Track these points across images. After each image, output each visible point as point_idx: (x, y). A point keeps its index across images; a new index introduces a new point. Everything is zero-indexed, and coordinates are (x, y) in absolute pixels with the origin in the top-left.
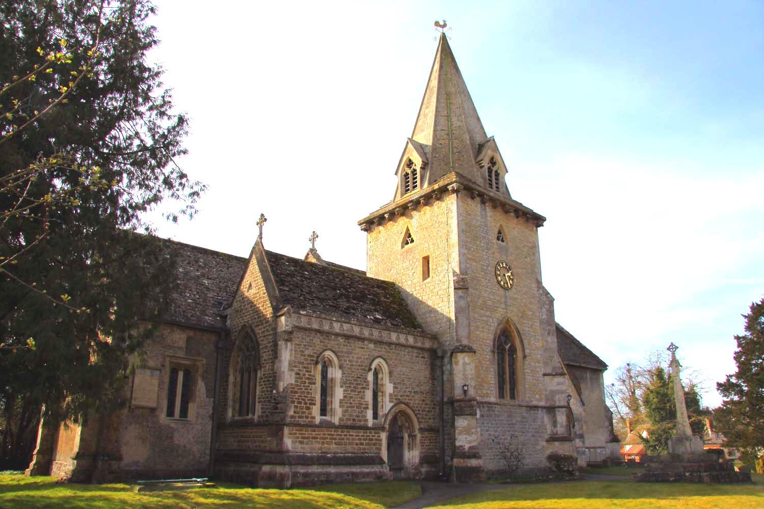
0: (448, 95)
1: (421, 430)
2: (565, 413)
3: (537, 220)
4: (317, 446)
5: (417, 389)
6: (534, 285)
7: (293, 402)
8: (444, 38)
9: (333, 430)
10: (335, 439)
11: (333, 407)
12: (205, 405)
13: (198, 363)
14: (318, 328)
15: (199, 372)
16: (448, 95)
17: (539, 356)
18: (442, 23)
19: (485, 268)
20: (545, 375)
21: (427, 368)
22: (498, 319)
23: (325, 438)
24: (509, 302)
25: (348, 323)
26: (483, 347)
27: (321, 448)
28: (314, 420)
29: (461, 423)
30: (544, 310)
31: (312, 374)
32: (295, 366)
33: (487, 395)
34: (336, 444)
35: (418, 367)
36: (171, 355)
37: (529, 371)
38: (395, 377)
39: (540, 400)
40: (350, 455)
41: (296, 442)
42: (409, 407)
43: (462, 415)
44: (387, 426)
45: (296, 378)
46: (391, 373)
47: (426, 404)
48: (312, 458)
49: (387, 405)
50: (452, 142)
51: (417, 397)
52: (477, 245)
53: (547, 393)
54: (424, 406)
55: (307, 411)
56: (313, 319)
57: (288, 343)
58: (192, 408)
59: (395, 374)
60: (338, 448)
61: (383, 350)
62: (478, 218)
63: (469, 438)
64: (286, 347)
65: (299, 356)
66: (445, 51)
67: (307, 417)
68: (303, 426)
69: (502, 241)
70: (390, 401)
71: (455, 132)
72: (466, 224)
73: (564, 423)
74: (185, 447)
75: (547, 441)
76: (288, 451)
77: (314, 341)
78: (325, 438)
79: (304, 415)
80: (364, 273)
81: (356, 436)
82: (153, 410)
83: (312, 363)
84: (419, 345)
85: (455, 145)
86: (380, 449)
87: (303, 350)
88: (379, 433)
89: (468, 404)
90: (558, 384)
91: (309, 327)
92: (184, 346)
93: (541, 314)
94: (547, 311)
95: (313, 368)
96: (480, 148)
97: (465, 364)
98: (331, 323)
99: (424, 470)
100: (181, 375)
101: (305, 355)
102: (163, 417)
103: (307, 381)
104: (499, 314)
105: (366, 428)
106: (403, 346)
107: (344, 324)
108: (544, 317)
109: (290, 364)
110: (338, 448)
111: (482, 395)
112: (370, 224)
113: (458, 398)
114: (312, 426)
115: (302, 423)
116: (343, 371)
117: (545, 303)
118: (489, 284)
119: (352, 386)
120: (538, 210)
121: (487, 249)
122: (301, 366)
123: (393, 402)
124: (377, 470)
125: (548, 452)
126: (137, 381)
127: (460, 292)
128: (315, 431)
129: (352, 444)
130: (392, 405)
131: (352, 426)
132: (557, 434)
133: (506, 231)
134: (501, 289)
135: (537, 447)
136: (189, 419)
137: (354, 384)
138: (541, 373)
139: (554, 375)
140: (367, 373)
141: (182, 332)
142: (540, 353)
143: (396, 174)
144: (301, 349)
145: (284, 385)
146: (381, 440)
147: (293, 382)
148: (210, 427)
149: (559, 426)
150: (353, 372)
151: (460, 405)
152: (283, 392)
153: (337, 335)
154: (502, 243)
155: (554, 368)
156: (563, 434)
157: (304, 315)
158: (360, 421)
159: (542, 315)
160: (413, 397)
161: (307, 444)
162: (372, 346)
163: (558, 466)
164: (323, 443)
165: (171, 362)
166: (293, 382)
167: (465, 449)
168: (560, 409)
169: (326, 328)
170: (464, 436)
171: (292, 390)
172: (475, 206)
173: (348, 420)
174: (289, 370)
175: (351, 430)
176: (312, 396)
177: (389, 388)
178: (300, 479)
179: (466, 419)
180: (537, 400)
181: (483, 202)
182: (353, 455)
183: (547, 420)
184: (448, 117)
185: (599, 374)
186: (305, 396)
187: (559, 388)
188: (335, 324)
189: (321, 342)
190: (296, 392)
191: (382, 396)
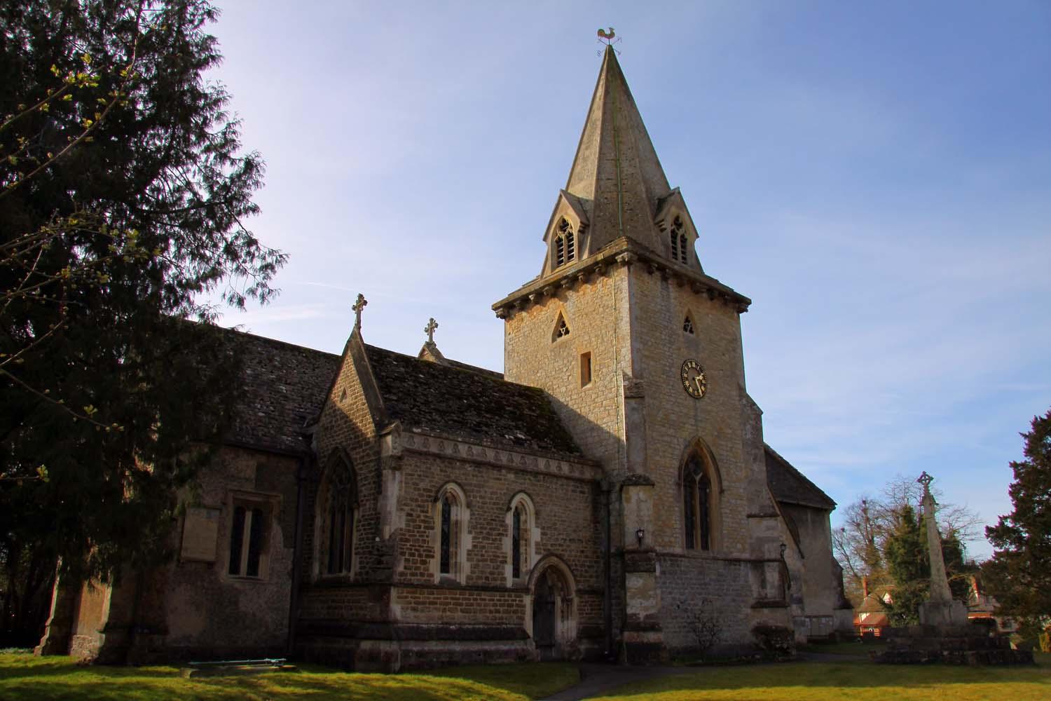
0: (617, 131)
1: (579, 592)
2: (777, 569)
3: (740, 303)
4: (437, 614)
5: (573, 536)
6: (735, 393)
7: (403, 554)
8: (610, 53)
9: (458, 592)
10: (461, 605)
11: (458, 561)
12: (283, 558)
16: (617, 131)
17: (742, 491)
18: (608, 32)
19: (668, 369)
20: (749, 516)
21: (588, 507)
23: (447, 604)
25: (478, 445)
27: (442, 618)
28: (432, 579)
30: (748, 427)
31: (429, 514)
32: (405, 505)
33: (670, 544)
34: (462, 611)
36: (236, 488)
37: (728, 511)
38: (544, 519)
39: (744, 550)
40: (481, 626)
41: (407, 608)
42: (563, 560)
44: (532, 587)
45: (408, 520)
46: (537, 513)
47: (586, 557)
48: (429, 631)
49: (532, 558)
51: (573, 546)
53: (753, 541)
54: (583, 559)
55: (422, 567)
57: (397, 472)
58: (264, 562)
60: (465, 617)
63: (646, 603)
64: (394, 478)
65: (412, 490)
66: (612, 70)
67: (422, 575)
68: (417, 586)
69: (691, 332)
70: (536, 553)
71: (625, 182)
73: (776, 583)
74: (254, 615)
76: (396, 622)
77: (433, 470)
78: (447, 604)
79: (418, 572)
81: (490, 600)
82: (210, 565)
83: (429, 499)
84: (577, 474)
86: (523, 619)
87: (417, 481)
88: (521, 597)
90: (768, 529)
91: (425, 450)
93: (744, 433)
94: (753, 428)
95: (430, 507)
96: (660, 204)
97: (639, 501)
98: (455, 445)
99: (583, 647)
100: (249, 517)
101: (419, 489)
102: (224, 575)
103: (423, 525)
105: (503, 589)
107: (472, 446)
108: (749, 436)
109: (398, 501)
110: (465, 617)
111: (663, 544)
113: (631, 548)
114: (429, 586)
115: (416, 583)
116: (471, 510)
118: (672, 391)
119: (485, 531)
120: (740, 289)
121: (670, 342)
122: (414, 504)
123: (540, 553)
124: (518, 647)
125: (754, 623)
126: (188, 524)
127: (633, 402)
128: (433, 594)
129: (484, 612)
130: (539, 557)
131: (484, 587)
132: (766, 597)
134: (688, 398)
136: (259, 577)
137: (487, 529)
138: (745, 513)
139: (762, 517)
140: (505, 514)
143: (545, 239)
145: (390, 530)
146: (524, 606)
147: (403, 526)
149: (768, 586)
150: (485, 512)
152: (389, 540)
153: (464, 461)
154: (691, 335)
155: (762, 507)
156: (775, 598)
158: (495, 579)
159: (746, 434)
160: (568, 546)
161: (422, 611)
162: (511, 476)
164: (444, 610)
166: (403, 526)
167: (639, 618)
168: (771, 564)
169: (449, 451)
170: (639, 601)
174: (397, 510)
175: (483, 593)
176: (430, 545)
177: (535, 534)
178: (413, 660)
179: (641, 577)
181: (665, 279)
182: (486, 627)
183: (752, 578)
186: (419, 546)
187: (768, 534)
188: (461, 447)
189: (441, 471)
190: (407, 540)
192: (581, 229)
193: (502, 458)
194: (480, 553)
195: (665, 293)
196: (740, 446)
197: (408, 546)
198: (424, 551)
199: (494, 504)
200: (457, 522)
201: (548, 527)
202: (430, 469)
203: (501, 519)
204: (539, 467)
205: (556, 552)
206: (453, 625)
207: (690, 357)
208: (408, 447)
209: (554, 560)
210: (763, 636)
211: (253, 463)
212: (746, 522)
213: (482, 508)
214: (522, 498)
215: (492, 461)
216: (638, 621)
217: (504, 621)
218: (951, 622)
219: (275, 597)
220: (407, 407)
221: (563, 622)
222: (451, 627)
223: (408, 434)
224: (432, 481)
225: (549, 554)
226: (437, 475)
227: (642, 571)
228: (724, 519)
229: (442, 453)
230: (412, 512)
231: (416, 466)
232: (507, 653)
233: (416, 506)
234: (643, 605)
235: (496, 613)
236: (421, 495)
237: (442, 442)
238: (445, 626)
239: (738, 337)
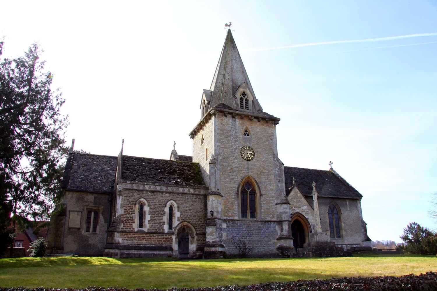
0: (226, 63)
1: (197, 234)
2: (287, 224)
3: (275, 121)
4: (135, 241)
5: (195, 215)
6: (271, 157)
7: (123, 222)
8: (229, 32)
9: (144, 234)
10: (146, 238)
11: (145, 224)
12: (103, 227)
13: (100, 208)
14: (136, 188)
15: (101, 212)
16: (226, 63)
17: (273, 194)
18: (229, 24)
19: (233, 151)
20: (276, 204)
21: (202, 204)
23: (140, 238)
24: (250, 167)
25: (153, 185)
26: (230, 191)
27: (138, 242)
28: (134, 230)
29: (209, 230)
30: (277, 169)
31: (133, 209)
32: (124, 206)
33: (232, 216)
34: (146, 240)
35: (196, 204)
36: (87, 205)
37: (264, 203)
38: (182, 209)
39: (273, 217)
40: (153, 246)
41: (124, 239)
42: (190, 223)
43: (209, 226)
44: (176, 233)
45: (124, 211)
46: (178, 207)
47: (201, 222)
49: (176, 223)
50: (223, 88)
51: (195, 218)
52: (228, 140)
53: (278, 214)
54: (199, 223)
55: (130, 226)
56: (134, 185)
57: (121, 196)
58: (98, 228)
59: (182, 207)
60: (147, 242)
61: (174, 197)
62: (230, 126)
63: (212, 237)
64: (120, 198)
65: (127, 202)
66: (230, 41)
67: (130, 229)
68: (128, 232)
69: (248, 135)
70: (178, 221)
71: (225, 82)
72: (221, 130)
73: (287, 230)
74: (94, 244)
75: (277, 239)
77: (134, 195)
78: (140, 238)
79: (129, 228)
80: (191, 158)
81: (157, 237)
82: (79, 229)
83: (133, 204)
84: (197, 193)
85: (225, 89)
86: (172, 244)
87: (129, 199)
88: (171, 236)
89: (213, 220)
90: (284, 208)
91: (132, 188)
92: (93, 201)
93: (275, 171)
94: (278, 170)
95: (133, 207)
96: (235, 89)
97: (213, 201)
98: (144, 186)
99: (197, 254)
100: (93, 214)
101: (129, 201)
102: (84, 232)
103: (130, 213)
104: (243, 174)
105: (163, 233)
106: (186, 194)
107: (151, 186)
108: (277, 173)
109: (121, 205)
110: (147, 242)
111: (228, 216)
112: (193, 134)
113: (209, 218)
114: (133, 232)
115: (127, 231)
116: (150, 207)
117: (277, 165)
118: (235, 159)
119: (156, 214)
120: (276, 115)
121: (235, 141)
122: (127, 206)
123: (179, 221)
124: (169, 253)
125: (278, 245)
126: (71, 217)
127: (212, 165)
128: (134, 235)
129: (155, 240)
130: (179, 222)
131: (156, 232)
132: (283, 235)
133: (250, 130)
134: (244, 161)
135: (270, 243)
136: (96, 233)
137: (157, 213)
138: (274, 203)
139: (281, 204)
140: (164, 208)
141: (92, 195)
142: (274, 192)
143: (200, 108)
144: (127, 198)
145: (118, 215)
146: (172, 239)
147: (123, 213)
148: (106, 236)
149: (284, 231)
150: (156, 207)
151: (209, 221)
152: (117, 218)
153: (147, 191)
154: (248, 136)
155: (282, 200)
156: (286, 235)
157: (129, 183)
158: (160, 230)
159: (276, 172)
160: (193, 218)
161: (130, 240)
162: (167, 195)
163: (282, 253)
164: (139, 240)
165: (87, 209)
166: (123, 213)
167: (210, 243)
168: (285, 222)
169: (141, 188)
170: (210, 236)
171: (122, 217)
172: (228, 120)
174: (121, 208)
175: (154, 234)
176: (133, 219)
177: (177, 214)
178: (125, 256)
179: (211, 228)
180: (271, 218)
181: (233, 117)
182: (155, 246)
183: (277, 228)
184: (224, 74)
185: (357, 202)
186: (129, 219)
187: (284, 210)
188: (146, 186)
189: (138, 195)
190: (125, 218)
191: (174, 218)
192: (208, 103)
193: (163, 189)
194: (153, 221)
195: (234, 122)
196: (273, 177)
197: (125, 220)
198: (131, 221)
199: (160, 205)
200: (145, 211)
201: (183, 212)
202: (134, 194)
203: (162, 210)
204: (180, 191)
205: (187, 220)
206: (142, 245)
207: (246, 145)
208: (125, 188)
209: (186, 223)
210: (281, 250)
211: (93, 197)
212: (275, 206)
213: (155, 206)
214: (172, 202)
215: (159, 190)
216: (210, 244)
217: (164, 244)
218: (316, 241)
219: (101, 239)
220: (132, 175)
221: (191, 245)
222: (141, 246)
223: (125, 184)
224: (134, 198)
225: (184, 221)
226: (137, 196)
227: (211, 226)
228: (262, 206)
229: (138, 189)
230: (126, 209)
231: (128, 194)
232: (163, 255)
233: (128, 206)
234: (211, 238)
235: (160, 241)
236: (130, 203)
237: (138, 185)
238: (139, 245)
239: (274, 134)
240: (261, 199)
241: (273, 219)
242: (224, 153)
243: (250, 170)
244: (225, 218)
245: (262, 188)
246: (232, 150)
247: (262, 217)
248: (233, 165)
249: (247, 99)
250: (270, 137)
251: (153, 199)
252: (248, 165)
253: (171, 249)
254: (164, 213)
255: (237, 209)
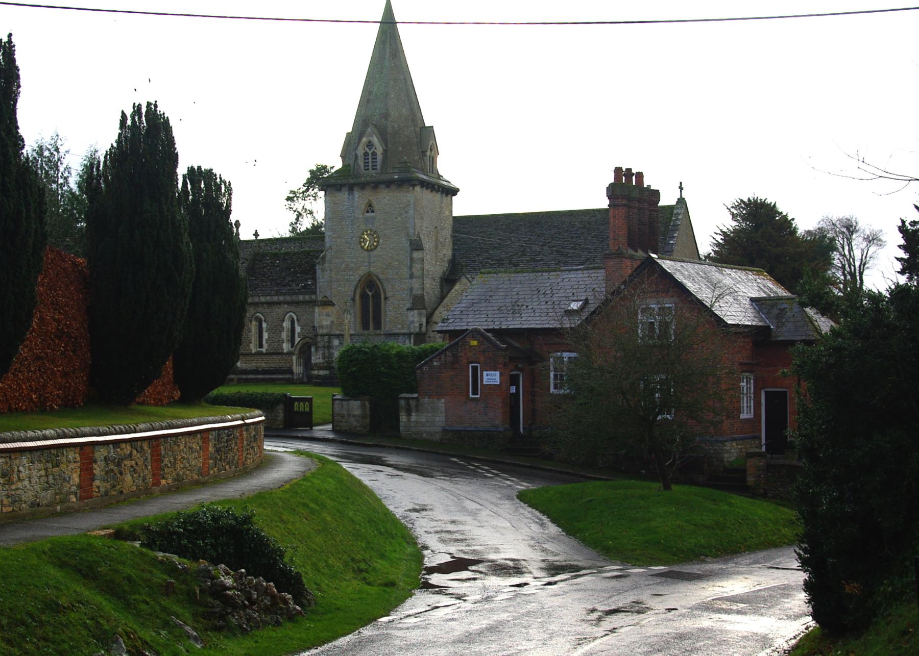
19: (350, 240)
22: (360, 275)
37: (390, 308)
39: (403, 328)
44: (296, 352)
46: (298, 320)
48: (249, 371)
62: (346, 203)
69: (373, 212)
73: (268, 392)
76: (238, 368)
86: (292, 365)
105: (282, 354)
114: (251, 354)
130: (299, 339)
134: (364, 252)
146: (293, 360)
154: (372, 214)
162: (286, 306)
173: (272, 349)
177: (298, 329)
209: (308, 340)
240: (386, 303)
241: (403, 331)
242: (337, 246)
243: (372, 264)
244: (338, 332)
245: (388, 287)
246: (348, 238)
247: (387, 329)
248: (349, 260)
249: (374, 152)
250: (404, 208)
251: (270, 312)
252: (370, 257)
253: (290, 371)
254: (283, 328)
255: (353, 320)
